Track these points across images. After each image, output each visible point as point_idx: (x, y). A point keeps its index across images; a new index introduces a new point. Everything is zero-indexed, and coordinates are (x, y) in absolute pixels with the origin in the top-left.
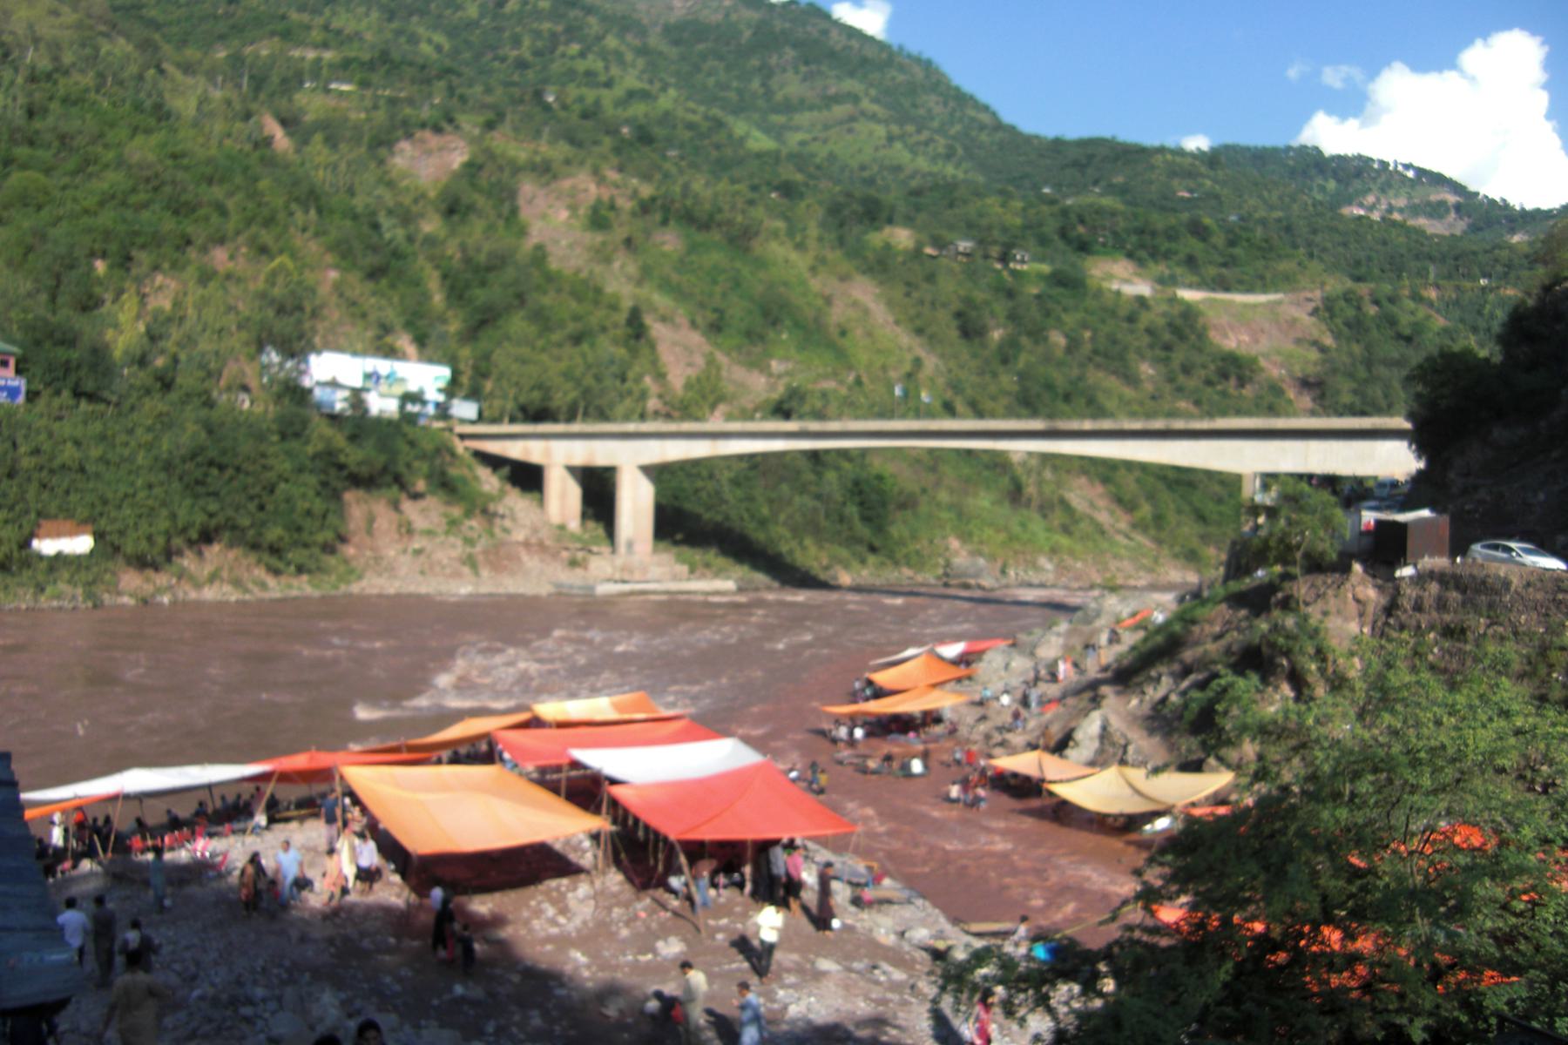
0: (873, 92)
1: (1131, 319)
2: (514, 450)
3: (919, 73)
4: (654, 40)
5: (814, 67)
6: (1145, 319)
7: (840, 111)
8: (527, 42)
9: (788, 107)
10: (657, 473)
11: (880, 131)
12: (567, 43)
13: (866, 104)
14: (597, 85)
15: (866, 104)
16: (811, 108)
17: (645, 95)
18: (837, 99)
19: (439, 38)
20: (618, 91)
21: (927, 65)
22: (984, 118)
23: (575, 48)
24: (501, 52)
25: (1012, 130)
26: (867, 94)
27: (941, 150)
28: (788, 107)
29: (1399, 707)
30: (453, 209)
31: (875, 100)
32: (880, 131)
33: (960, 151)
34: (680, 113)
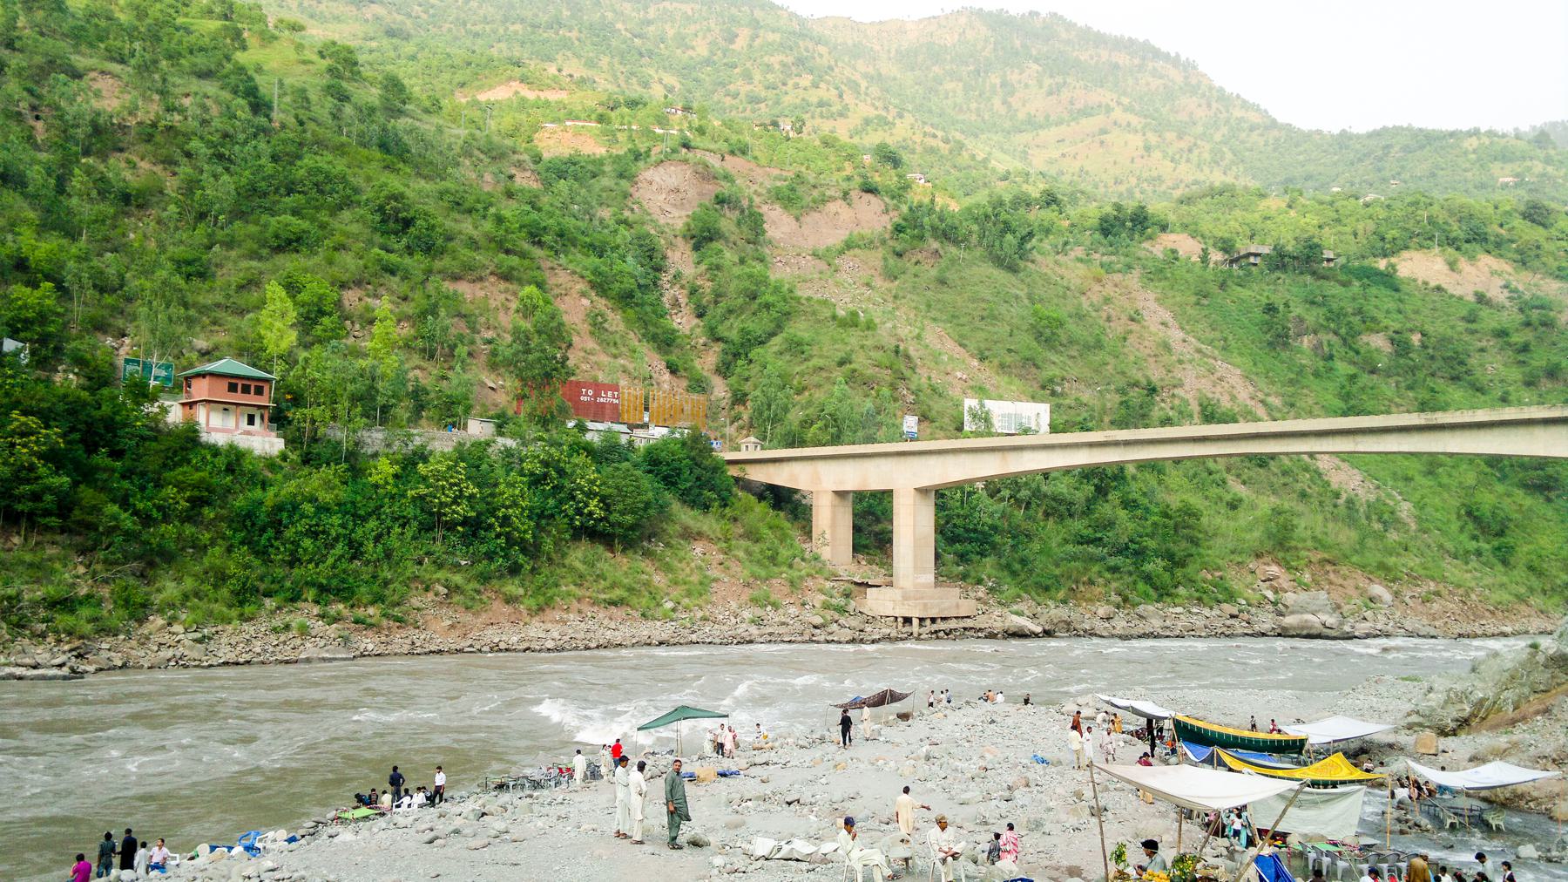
0: (1126, 101)
1: (1471, 319)
2: (780, 477)
3: (1176, 76)
4: (889, 69)
5: (1059, 79)
6: (1489, 320)
7: (1090, 124)
8: (757, 76)
9: (1032, 124)
10: (940, 496)
11: (1136, 141)
12: (23, 512)
13: (1118, 114)
14: (832, 116)
15: (1118, 114)
16: (1058, 123)
17: (884, 123)
18: (1086, 112)
19: (670, 80)
20: (854, 120)
21: (1188, 67)
22: (1253, 117)
23: (806, 80)
24: (732, 88)
25: (1288, 128)
26: (1119, 103)
27: (1207, 156)
28: (1032, 124)
29: (810, 583)
30: (702, 238)
31: (1128, 109)
32: (1136, 141)
33: (1229, 156)
34: (918, 138)
